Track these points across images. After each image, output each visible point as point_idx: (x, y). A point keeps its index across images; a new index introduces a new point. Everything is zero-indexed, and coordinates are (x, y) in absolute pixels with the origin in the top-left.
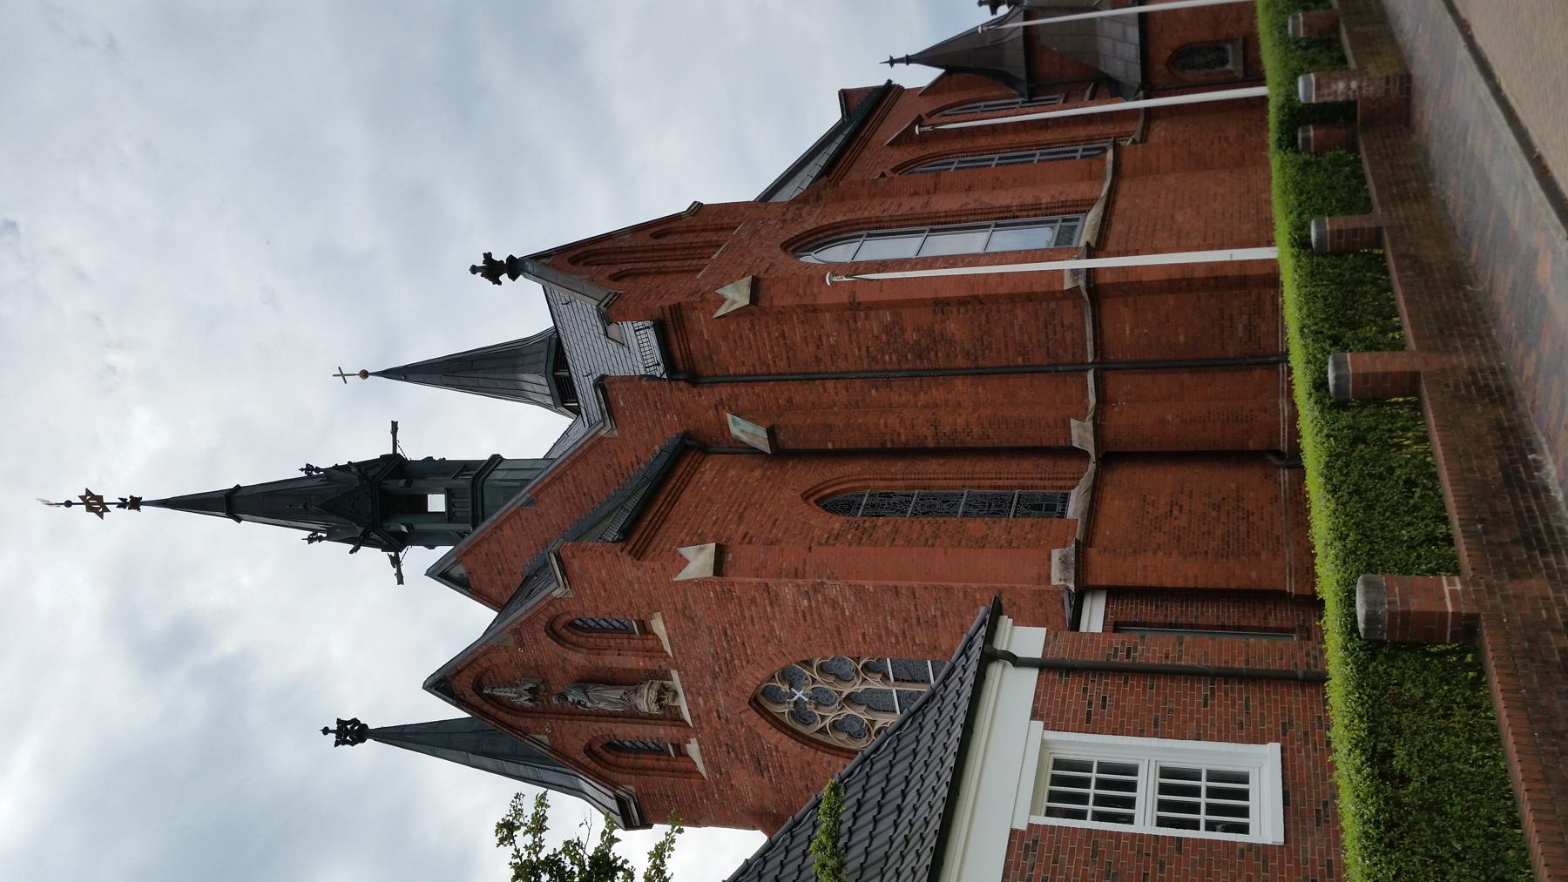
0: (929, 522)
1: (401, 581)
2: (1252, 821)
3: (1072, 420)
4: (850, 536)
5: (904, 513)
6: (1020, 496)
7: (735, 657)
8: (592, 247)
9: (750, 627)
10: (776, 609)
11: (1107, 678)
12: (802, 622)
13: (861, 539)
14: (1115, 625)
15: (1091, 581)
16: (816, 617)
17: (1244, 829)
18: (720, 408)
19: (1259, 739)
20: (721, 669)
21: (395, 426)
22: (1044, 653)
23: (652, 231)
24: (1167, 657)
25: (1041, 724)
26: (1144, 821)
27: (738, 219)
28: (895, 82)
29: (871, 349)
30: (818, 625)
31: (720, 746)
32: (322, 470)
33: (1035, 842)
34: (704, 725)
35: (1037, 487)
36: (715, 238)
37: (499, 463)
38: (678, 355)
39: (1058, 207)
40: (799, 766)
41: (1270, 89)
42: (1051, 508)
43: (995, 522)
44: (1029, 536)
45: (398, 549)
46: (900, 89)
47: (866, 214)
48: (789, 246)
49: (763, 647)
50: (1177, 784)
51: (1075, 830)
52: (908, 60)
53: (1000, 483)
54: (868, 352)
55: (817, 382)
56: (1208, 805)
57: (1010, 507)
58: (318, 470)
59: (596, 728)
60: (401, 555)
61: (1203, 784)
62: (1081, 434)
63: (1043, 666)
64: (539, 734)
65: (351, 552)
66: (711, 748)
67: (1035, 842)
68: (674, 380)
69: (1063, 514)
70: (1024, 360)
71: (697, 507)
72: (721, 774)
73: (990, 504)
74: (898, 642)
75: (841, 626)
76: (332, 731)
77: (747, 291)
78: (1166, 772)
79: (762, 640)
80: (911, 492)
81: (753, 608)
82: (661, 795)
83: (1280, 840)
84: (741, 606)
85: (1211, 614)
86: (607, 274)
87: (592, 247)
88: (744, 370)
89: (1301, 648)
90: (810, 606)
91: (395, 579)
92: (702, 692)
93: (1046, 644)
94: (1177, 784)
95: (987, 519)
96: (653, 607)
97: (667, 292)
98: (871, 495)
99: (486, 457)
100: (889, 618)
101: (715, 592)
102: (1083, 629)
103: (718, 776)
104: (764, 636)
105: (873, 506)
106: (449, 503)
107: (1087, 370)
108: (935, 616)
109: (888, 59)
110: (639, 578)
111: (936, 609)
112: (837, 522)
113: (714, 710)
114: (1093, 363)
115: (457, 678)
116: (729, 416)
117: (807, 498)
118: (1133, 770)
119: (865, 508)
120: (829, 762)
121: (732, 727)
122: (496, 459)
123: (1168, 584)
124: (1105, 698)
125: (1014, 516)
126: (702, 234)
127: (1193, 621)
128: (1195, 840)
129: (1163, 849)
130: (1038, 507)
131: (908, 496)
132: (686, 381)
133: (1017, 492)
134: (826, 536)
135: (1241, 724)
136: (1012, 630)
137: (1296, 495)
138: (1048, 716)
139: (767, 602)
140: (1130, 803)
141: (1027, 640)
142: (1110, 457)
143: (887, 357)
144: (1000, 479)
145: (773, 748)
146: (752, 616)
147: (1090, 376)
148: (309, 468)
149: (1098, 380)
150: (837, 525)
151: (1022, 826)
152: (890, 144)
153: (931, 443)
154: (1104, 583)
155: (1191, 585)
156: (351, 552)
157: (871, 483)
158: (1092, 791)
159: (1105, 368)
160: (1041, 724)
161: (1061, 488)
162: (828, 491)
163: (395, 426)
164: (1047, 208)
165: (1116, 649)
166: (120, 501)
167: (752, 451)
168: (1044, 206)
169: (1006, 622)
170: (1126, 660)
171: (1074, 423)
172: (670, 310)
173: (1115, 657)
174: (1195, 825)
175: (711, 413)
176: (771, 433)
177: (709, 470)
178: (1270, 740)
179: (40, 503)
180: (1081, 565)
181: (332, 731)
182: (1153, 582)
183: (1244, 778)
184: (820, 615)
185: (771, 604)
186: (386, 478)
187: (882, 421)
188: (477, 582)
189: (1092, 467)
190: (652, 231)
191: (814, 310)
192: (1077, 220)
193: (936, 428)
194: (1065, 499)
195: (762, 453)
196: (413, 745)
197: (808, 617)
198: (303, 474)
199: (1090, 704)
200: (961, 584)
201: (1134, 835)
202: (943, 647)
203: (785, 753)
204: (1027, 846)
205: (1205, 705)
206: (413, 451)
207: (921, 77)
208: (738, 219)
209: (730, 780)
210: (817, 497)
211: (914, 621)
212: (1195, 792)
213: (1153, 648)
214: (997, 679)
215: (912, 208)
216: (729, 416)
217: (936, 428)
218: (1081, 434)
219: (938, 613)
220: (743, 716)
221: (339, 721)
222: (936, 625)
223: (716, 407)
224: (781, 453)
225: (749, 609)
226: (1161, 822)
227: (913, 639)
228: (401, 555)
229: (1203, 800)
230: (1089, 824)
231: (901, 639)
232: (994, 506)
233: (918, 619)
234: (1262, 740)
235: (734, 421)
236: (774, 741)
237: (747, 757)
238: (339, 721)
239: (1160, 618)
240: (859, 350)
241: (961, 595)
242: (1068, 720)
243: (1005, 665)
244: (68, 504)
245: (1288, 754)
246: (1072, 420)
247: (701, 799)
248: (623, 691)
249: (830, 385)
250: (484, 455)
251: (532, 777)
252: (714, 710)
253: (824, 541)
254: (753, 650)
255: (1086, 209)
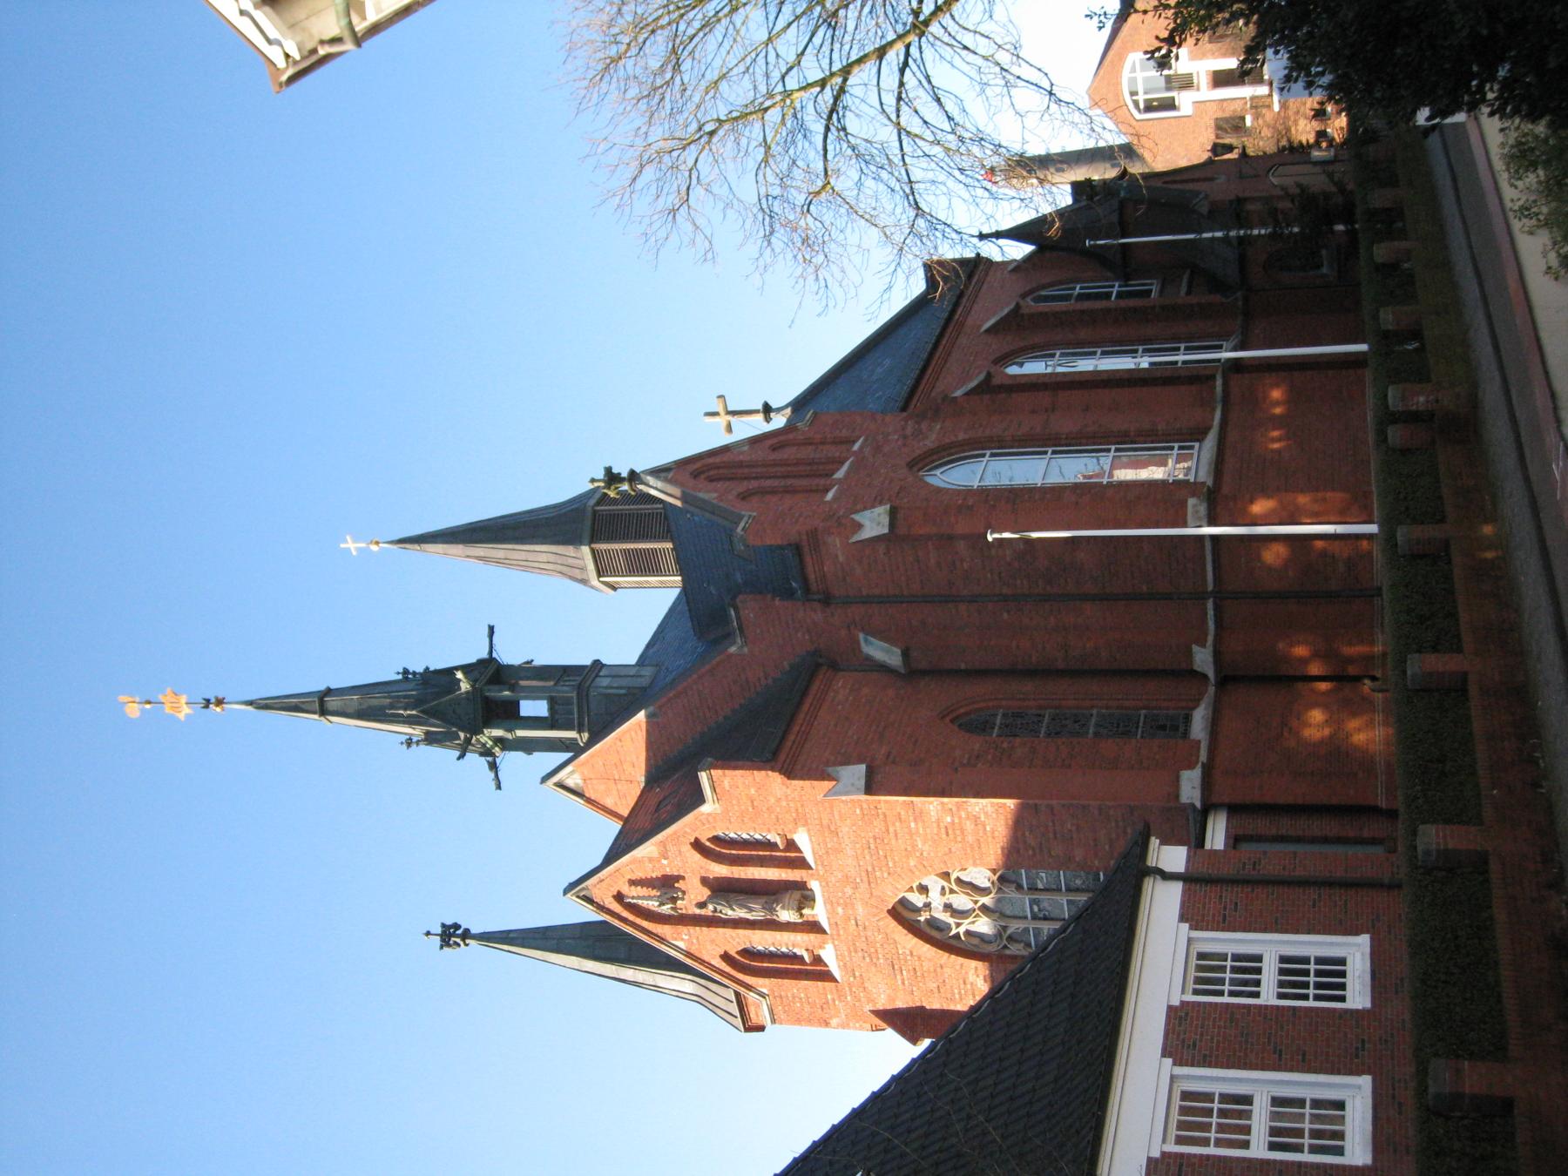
0: (1063, 743)
1: (499, 787)
2: (1348, 993)
3: (1193, 646)
4: (990, 757)
5: (1036, 733)
6: (1146, 716)
7: (877, 869)
8: (711, 460)
9: (893, 842)
10: (920, 824)
11: (1238, 887)
12: (944, 836)
13: (1001, 759)
14: (1235, 840)
15: (1215, 799)
16: (958, 832)
17: (1342, 999)
18: (852, 627)
19: (1355, 931)
20: (862, 880)
21: (491, 630)
22: (1187, 867)
23: (770, 442)
24: (1284, 869)
25: (1187, 925)
26: (1268, 994)
27: (857, 433)
28: (984, 254)
29: (1003, 575)
30: (959, 839)
31: (856, 952)
33: (1187, 1014)
34: (841, 932)
35: (1160, 708)
36: (837, 454)
37: (601, 669)
38: (812, 577)
39: (1174, 434)
40: (932, 969)
41: (1369, 345)
42: (1175, 728)
43: (1125, 744)
44: (1157, 757)
46: (989, 262)
47: (988, 433)
48: (913, 466)
49: (904, 860)
50: (1292, 968)
51: (1216, 1004)
52: (998, 235)
53: (1127, 703)
54: (1000, 578)
55: (950, 605)
56: (1309, 976)
57: (1137, 728)
59: (734, 935)
61: (1312, 967)
62: (1203, 659)
63: (1185, 878)
64: (676, 939)
65: (459, 759)
66: (846, 953)
67: (1187, 1014)
68: (808, 600)
69: (1186, 734)
70: (1148, 588)
71: (836, 725)
72: (855, 977)
73: (1118, 724)
74: (1034, 855)
75: (982, 840)
77: (886, 520)
78: (1283, 959)
79: (904, 853)
80: (1042, 712)
81: (897, 824)
82: (794, 997)
83: (1368, 1005)
84: (885, 821)
85: (1317, 826)
86: (735, 493)
87: (711, 460)
88: (877, 591)
89: (1388, 860)
90: (953, 821)
91: (493, 785)
92: (842, 901)
93: (1188, 861)
94: (1292, 968)
95: (1117, 740)
97: (800, 516)
98: (1004, 715)
99: (587, 662)
100: (1027, 834)
101: (862, 809)
102: (1208, 846)
103: (852, 979)
104: (906, 850)
105: (1007, 726)
106: (551, 709)
107: (1206, 599)
108: (1070, 831)
109: (977, 234)
110: (787, 796)
111: (1072, 825)
112: (977, 743)
113: (852, 918)
114: (1212, 592)
115: (598, 886)
116: (861, 636)
117: (943, 717)
118: (1259, 958)
119: (1000, 728)
120: (962, 965)
121: (869, 934)
122: (597, 663)
123: (1281, 801)
124: (1236, 904)
125: (1142, 737)
126: (821, 447)
127: (1300, 833)
128: (1306, 1008)
129: (1283, 1016)
130: (1163, 728)
131: (1040, 715)
132: (819, 601)
133: (1143, 712)
134: (967, 756)
135: (1341, 920)
136: (1159, 848)
138: (1192, 920)
139: (911, 818)
140: (1258, 983)
141: (1173, 857)
142: (1227, 680)
143: (1019, 582)
144: (1127, 699)
145: (908, 952)
146: (895, 831)
147: (1210, 604)
149: (1217, 608)
150: (977, 746)
151: (1176, 1002)
152: (988, 331)
153: (1061, 665)
154: (1227, 800)
155: (1300, 801)
156: (459, 759)
157: (1004, 703)
158: (1228, 975)
160: (1187, 925)
161: (1183, 708)
162: (962, 711)
163: (491, 630)
164: (1163, 435)
165: (1244, 863)
167: (883, 668)
168: (1160, 433)
169: (1154, 842)
170: (1252, 873)
171: (1195, 648)
172: (807, 534)
173: (1244, 868)
174: (1306, 997)
175: (843, 632)
176: (906, 654)
177: (841, 688)
178: (1362, 933)
180: (1207, 784)
182: (1267, 800)
183: (1342, 962)
184: (962, 831)
185: (915, 820)
187: (1014, 643)
188: (592, 791)
189: (1212, 690)
190: (770, 442)
191: (951, 538)
192: (1192, 448)
193: (1066, 651)
194: (1188, 719)
195: (900, 673)
197: (950, 832)
198: (400, 677)
199: (1225, 909)
200: (1098, 802)
201: (1261, 1006)
202: (1077, 859)
203: (919, 958)
204: (1181, 1018)
205: (1314, 906)
206: (510, 655)
207: (1018, 251)
208: (857, 433)
209: (863, 983)
210: (951, 716)
211: (1051, 835)
212: (1306, 973)
213: (1274, 859)
214: (1150, 893)
215: (1032, 428)
216: (861, 636)
217: (1066, 651)
218: (1203, 659)
219: (1074, 828)
220: (881, 923)
221: (443, 925)
222: (1072, 838)
223: (849, 627)
224: (912, 673)
225: (894, 824)
226: (1281, 996)
227: (1050, 852)
229: (1312, 979)
230: (1226, 999)
231: (1037, 851)
232: (1122, 727)
233: (1055, 834)
234: (1357, 933)
235: (866, 641)
236: (909, 946)
237: (882, 961)
238: (443, 925)
239: (1274, 832)
240: (992, 574)
241: (1096, 812)
242: (1208, 922)
243: (1155, 878)
245: (641, 803)
246: (1193, 646)
247: (834, 1000)
248: (764, 901)
249: (962, 607)
250: (587, 661)
252: (852, 918)
253: (965, 761)
254: (894, 863)
255: (1200, 437)
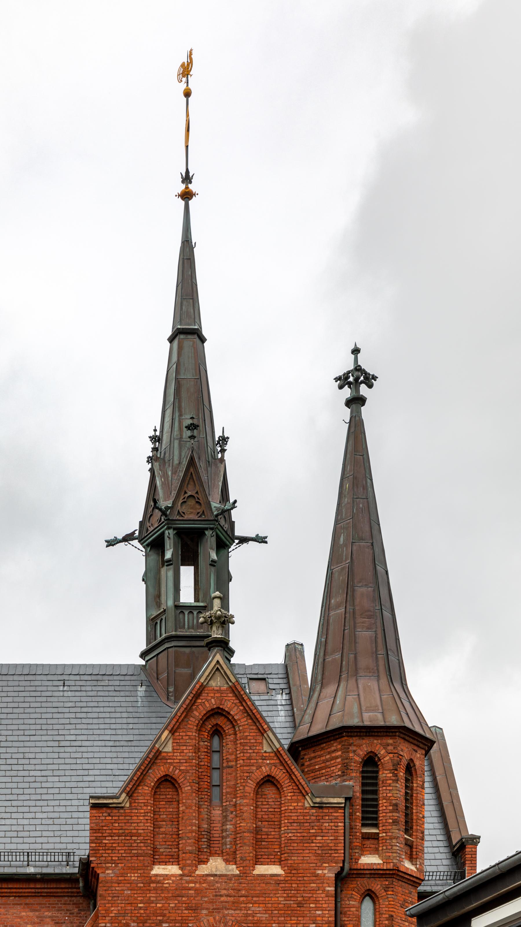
32: (223, 456)
45: (233, 538)
58: (223, 451)
60: (136, 543)
76: (155, 433)
91: (111, 537)
96: (291, 870)
137: (73, 913)
148: (224, 440)
159: (74, 861)
166: (191, 175)
179: (185, 59)
181: (155, 433)
186: (218, 537)
196: (371, 499)
198: (218, 434)
228: (136, 543)
244: (187, 94)
251: (321, 694)
